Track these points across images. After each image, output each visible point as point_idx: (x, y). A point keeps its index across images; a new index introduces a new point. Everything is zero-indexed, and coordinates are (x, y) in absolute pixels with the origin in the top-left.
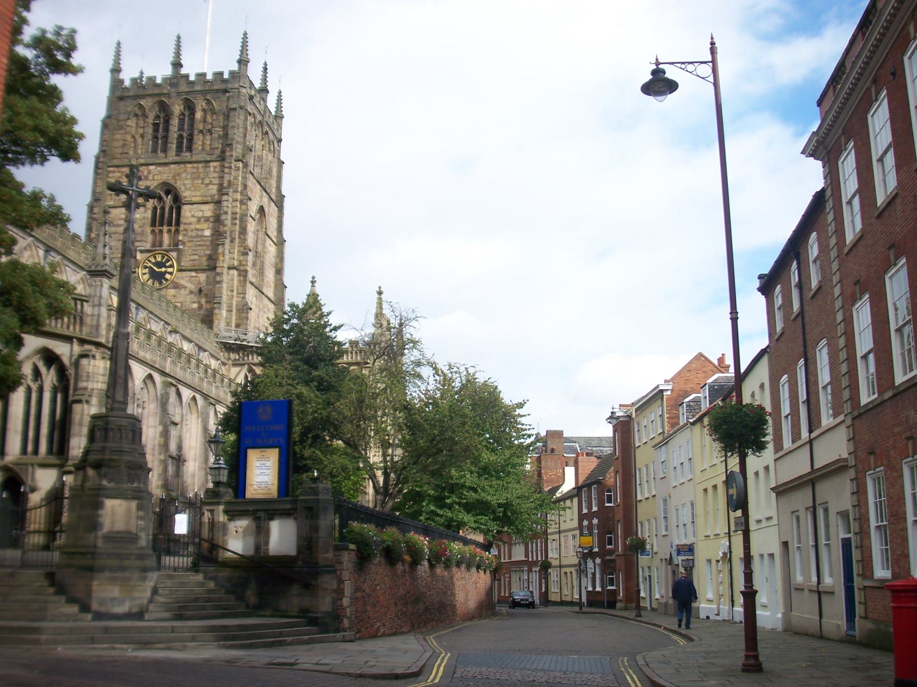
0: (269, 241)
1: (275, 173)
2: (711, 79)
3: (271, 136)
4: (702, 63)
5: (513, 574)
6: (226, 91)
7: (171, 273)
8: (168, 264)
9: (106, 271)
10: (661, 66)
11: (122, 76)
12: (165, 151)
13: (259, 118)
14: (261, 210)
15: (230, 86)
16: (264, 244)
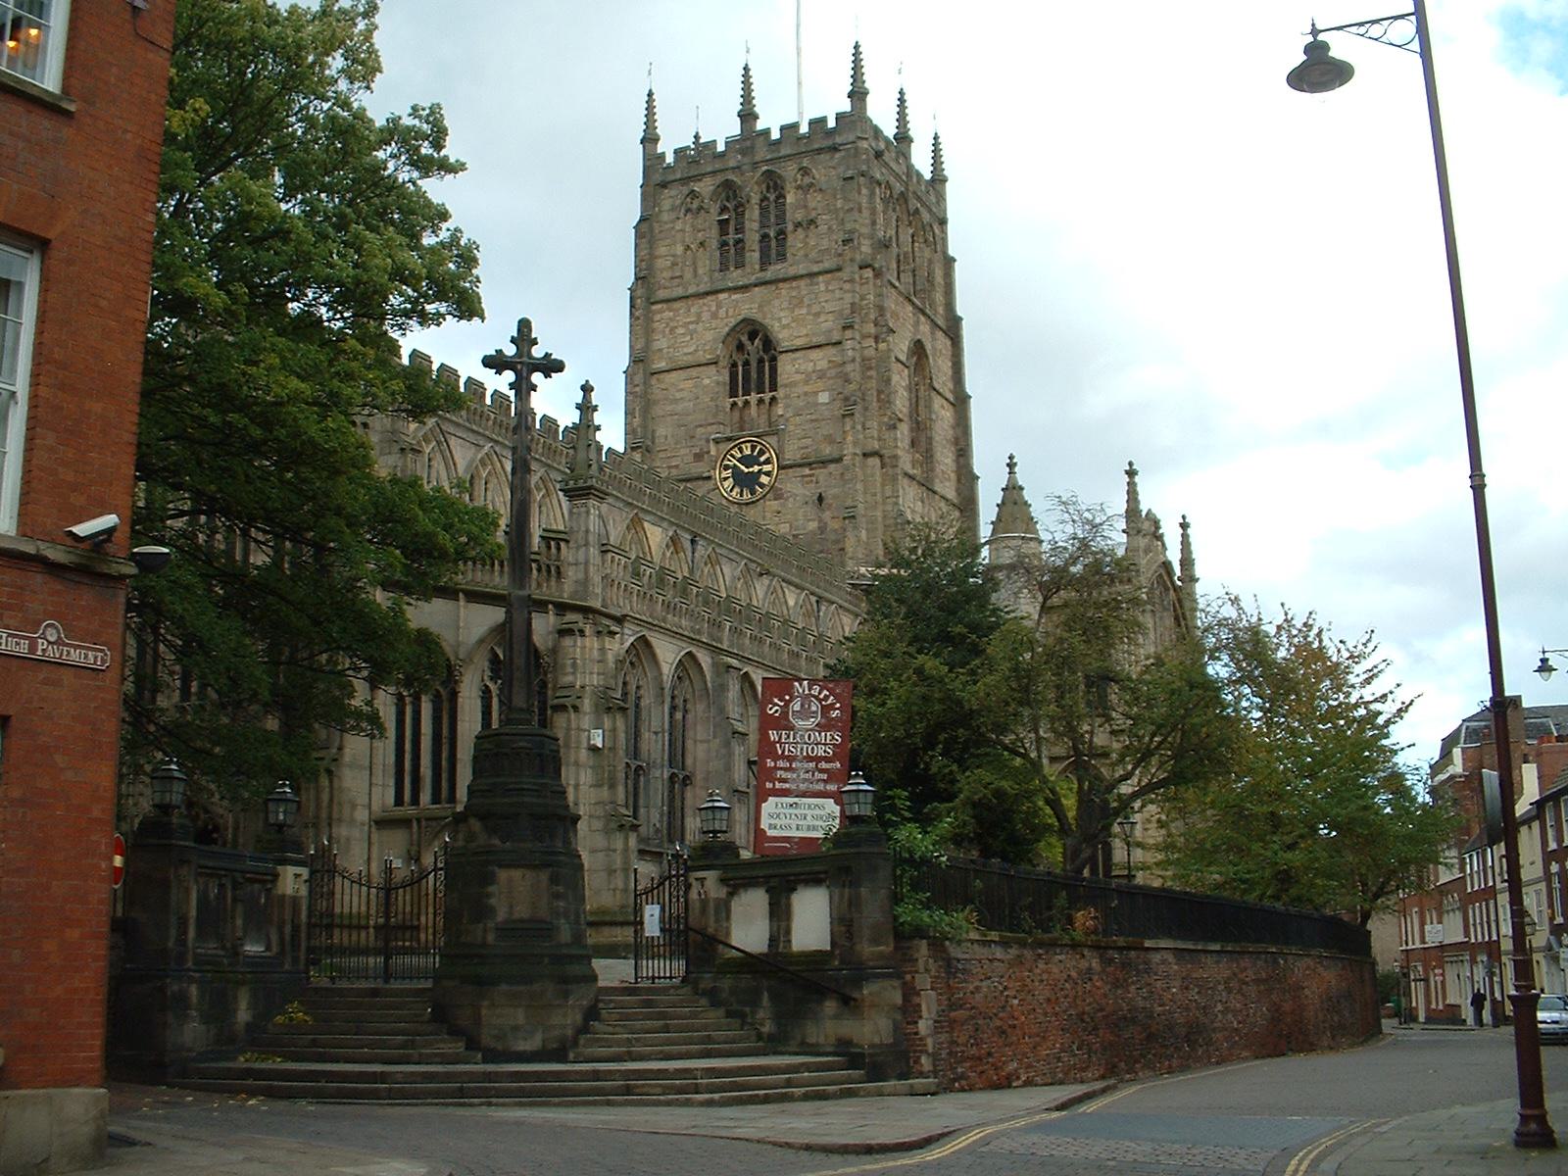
0: (938, 402)
1: (939, 279)
2: (1416, 46)
3: (926, 216)
4: (1396, 18)
5: (1448, 967)
6: (834, 149)
7: (768, 474)
8: (762, 459)
9: (591, 487)
10: (1321, 37)
12: (740, 265)
13: (898, 187)
14: (918, 349)
15: (838, 140)
16: (929, 407)
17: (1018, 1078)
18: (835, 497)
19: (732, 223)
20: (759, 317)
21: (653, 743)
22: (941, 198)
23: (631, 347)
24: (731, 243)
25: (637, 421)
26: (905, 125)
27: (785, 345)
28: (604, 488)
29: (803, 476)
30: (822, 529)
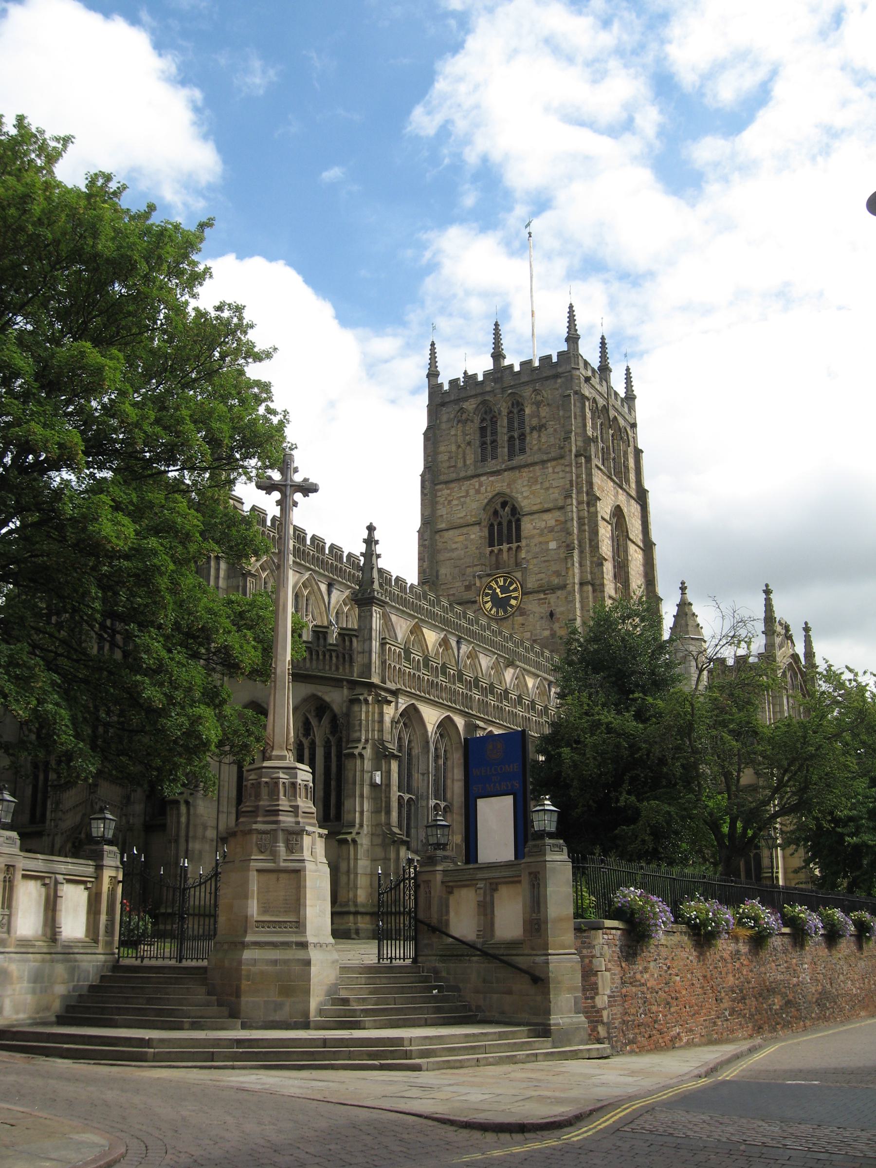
6: (557, 376)
7: (516, 598)
8: (511, 588)
11: (440, 380)
13: (601, 402)
14: (618, 512)
15: (560, 370)
16: (626, 551)
17: (681, 1039)
18: (562, 613)
19: (489, 429)
20: (508, 491)
21: (420, 780)
22: (632, 409)
23: (422, 515)
24: (489, 442)
25: (426, 564)
26: (606, 361)
27: (526, 510)
28: (383, 598)
29: (540, 599)
30: (553, 635)
